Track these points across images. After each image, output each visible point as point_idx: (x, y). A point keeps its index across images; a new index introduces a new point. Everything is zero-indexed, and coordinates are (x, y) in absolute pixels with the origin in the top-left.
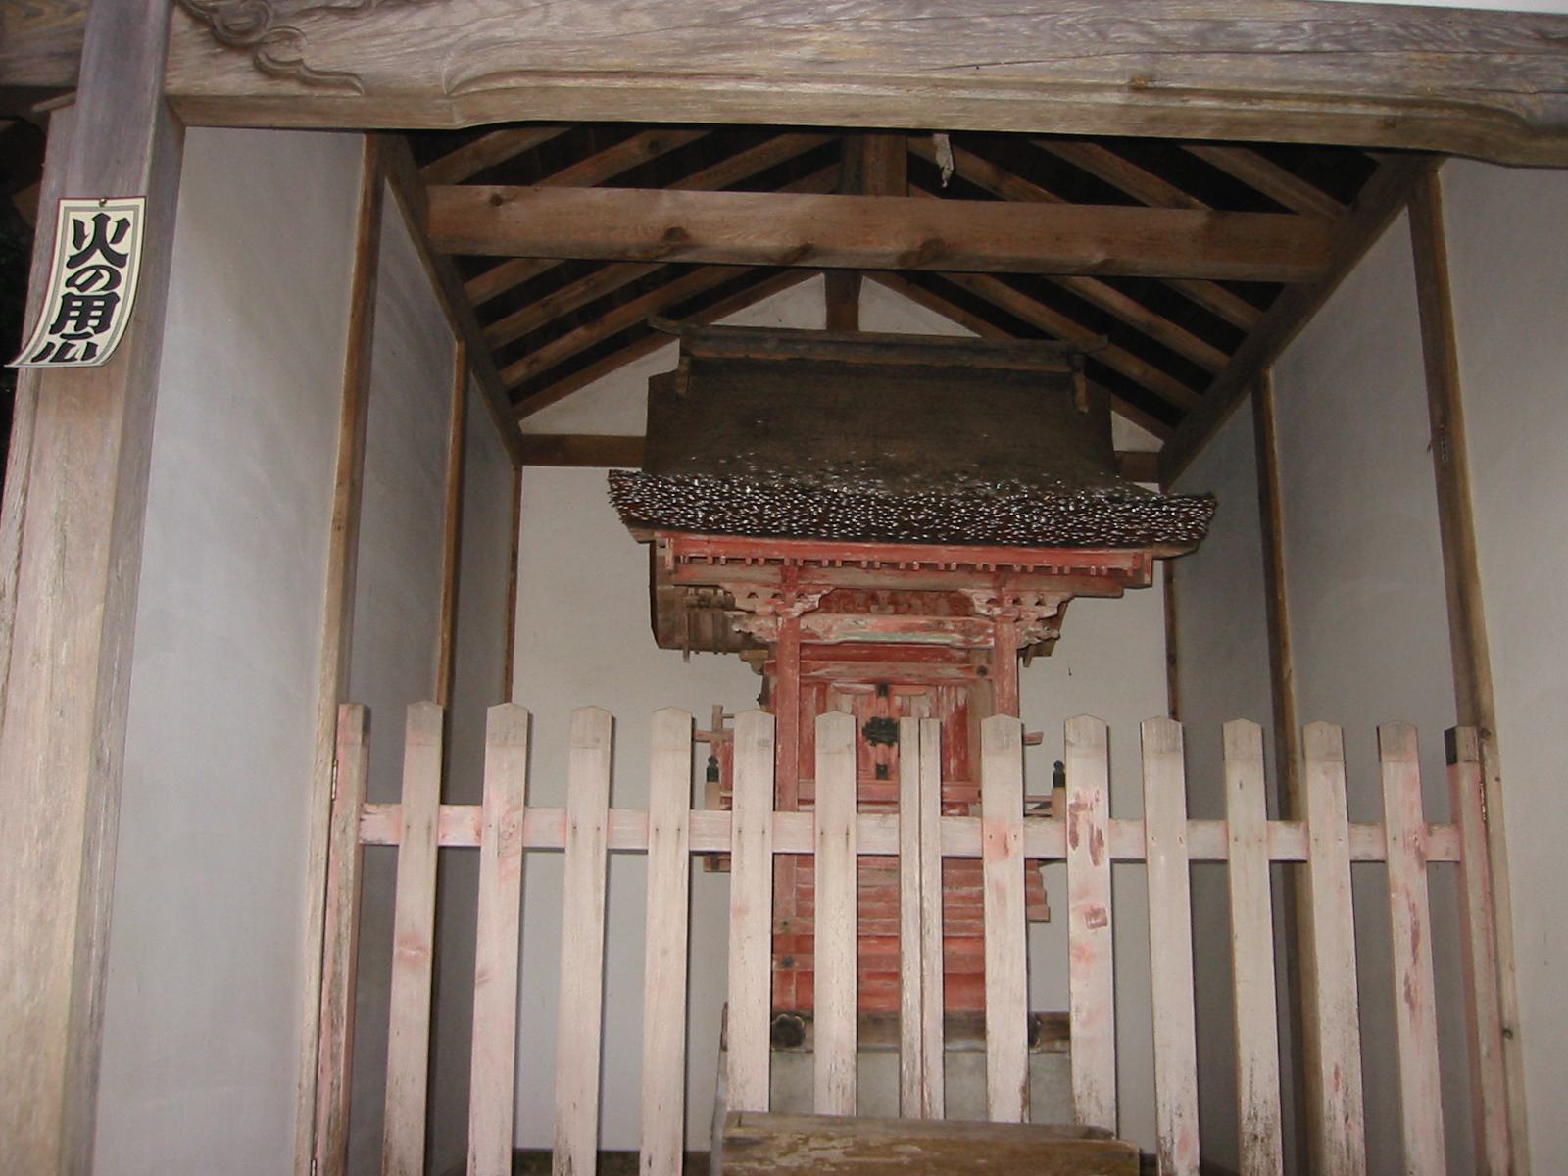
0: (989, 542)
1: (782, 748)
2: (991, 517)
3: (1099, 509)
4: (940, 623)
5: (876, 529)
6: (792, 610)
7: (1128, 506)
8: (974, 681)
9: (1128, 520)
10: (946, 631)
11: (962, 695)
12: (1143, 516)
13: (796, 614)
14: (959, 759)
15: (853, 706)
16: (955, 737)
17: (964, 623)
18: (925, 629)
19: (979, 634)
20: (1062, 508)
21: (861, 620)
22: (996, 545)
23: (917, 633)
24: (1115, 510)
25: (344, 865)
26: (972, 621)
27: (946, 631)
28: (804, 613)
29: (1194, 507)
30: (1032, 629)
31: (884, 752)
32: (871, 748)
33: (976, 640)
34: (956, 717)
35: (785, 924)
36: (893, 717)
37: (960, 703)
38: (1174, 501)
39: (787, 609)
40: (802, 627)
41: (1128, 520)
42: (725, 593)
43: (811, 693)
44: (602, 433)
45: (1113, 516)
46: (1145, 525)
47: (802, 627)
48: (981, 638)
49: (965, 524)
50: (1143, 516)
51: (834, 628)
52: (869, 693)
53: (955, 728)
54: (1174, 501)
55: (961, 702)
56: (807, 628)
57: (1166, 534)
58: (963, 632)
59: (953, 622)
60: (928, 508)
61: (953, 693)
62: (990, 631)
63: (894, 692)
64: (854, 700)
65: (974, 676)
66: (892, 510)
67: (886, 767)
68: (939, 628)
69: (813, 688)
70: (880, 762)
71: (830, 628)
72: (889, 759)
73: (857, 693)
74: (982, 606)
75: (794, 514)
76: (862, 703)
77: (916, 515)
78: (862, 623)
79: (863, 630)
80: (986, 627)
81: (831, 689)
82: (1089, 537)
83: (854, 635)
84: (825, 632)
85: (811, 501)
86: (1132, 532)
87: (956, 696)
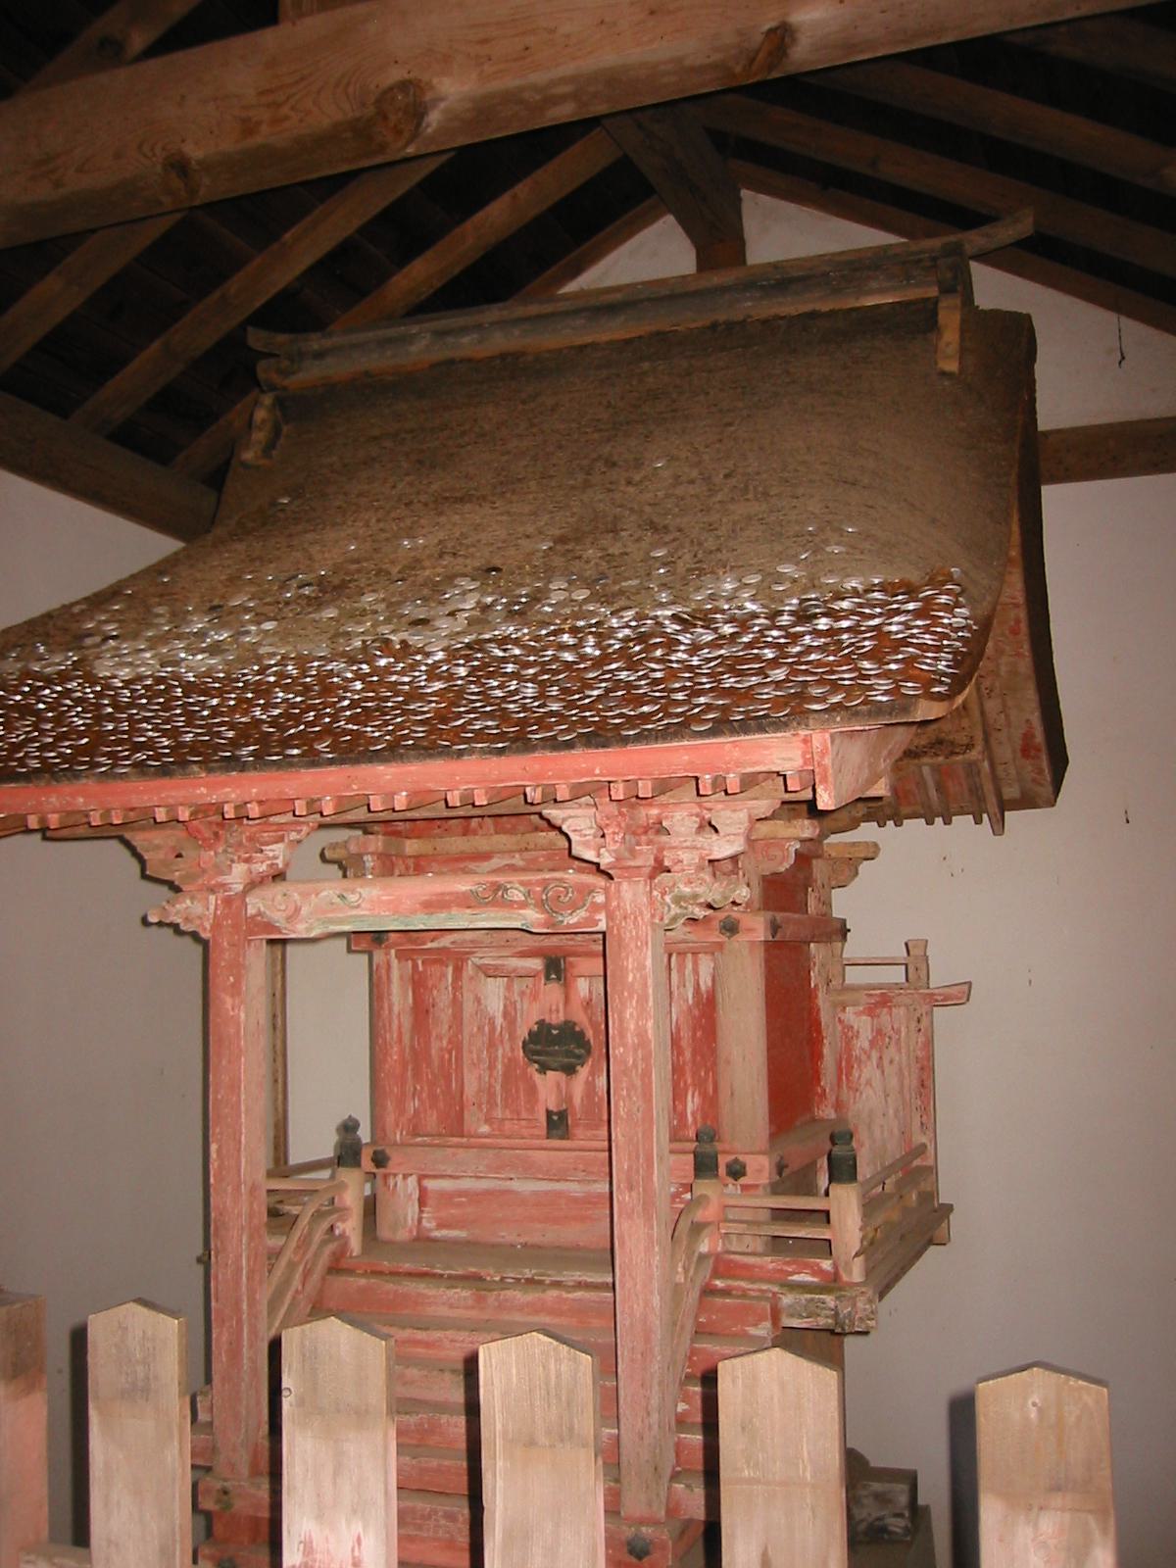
0: (427, 749)
1: (219, 1152)
2: (415, 694)
3: (656, 646)
4: (497, 887)
5: (194, 748)
6: (227, 879)
7: (728, 629)
8: (720, 946)
9: (733, 666)
10: (511, 904)
11: (706, 966)
12: (769, 654)
13: (240, 887)
14: (704, 1095)
15: (506, 998)
16: (694, 1053)
17: (545, 884)
18: (467, 901)
19: (574, 907)
20: (568, 657)
21: (353, 892)
22: (440, 754)
23: (454, 911)
24: (694, 648)
25: (479, 1029)
26: (561, 880)
27: (511, 904)
28: (254, 884)
29: (898, 612)
30: (687, 890)
31: (558, 1085)
32: (537, 1077)
33: (573, 920)
34: (696, 1012)
35: (225, 1492)
36: (575, 1019)
37: (703, 988)
38: (845, 605)
39: (221, 879)
40: (251, 911)
41: (733, 666)
42: (260, 803)
43: (444, 975)
44: (990, 269)
45: (695, 661)
46: (779, 674)
47: (251, 911)
48: (582, 913)
49: (365, 717)
50: (769, 654)
51: (304, 911)
52: (534, 976)
53: (694, 1034)
54: (845, 605)
55: (705, 982)
56: (260, 913)
57: (835, 687)
58: (541, 905)
59: (522, 883)
60: (286, 689)
61: (689, 966)
62: (600, 899)
63: (576, 972)
64: (509, 988)
65: (716, 937)
66: (215, 702)
67: (563, 1115)
68: (496, 896)
69: (447, 966)
70: (552, 1107)
71: (297, 910)
72: (569, 1099)
73: (511, 976)
74: (586, 844)
75: (43, 732)
76: (522, 994)
77: (265, 708)
78: (352, 898)
79: (354, 912)
80: (590, 890)
81: (469, 970)
82: (646, 718)
83: (341, 921)
84: (289, 919)
85: (68, 702)
86: (748, 694)
87: (696, 972)
